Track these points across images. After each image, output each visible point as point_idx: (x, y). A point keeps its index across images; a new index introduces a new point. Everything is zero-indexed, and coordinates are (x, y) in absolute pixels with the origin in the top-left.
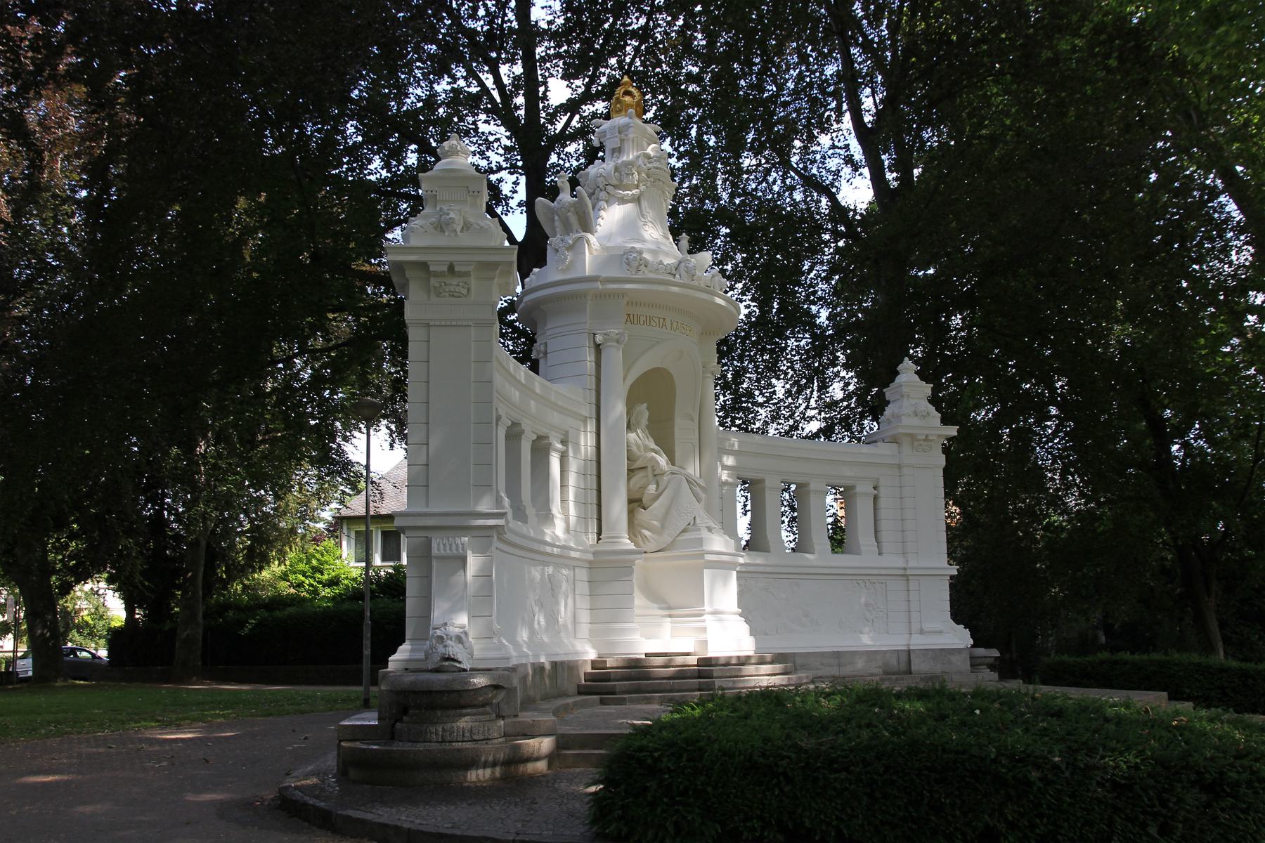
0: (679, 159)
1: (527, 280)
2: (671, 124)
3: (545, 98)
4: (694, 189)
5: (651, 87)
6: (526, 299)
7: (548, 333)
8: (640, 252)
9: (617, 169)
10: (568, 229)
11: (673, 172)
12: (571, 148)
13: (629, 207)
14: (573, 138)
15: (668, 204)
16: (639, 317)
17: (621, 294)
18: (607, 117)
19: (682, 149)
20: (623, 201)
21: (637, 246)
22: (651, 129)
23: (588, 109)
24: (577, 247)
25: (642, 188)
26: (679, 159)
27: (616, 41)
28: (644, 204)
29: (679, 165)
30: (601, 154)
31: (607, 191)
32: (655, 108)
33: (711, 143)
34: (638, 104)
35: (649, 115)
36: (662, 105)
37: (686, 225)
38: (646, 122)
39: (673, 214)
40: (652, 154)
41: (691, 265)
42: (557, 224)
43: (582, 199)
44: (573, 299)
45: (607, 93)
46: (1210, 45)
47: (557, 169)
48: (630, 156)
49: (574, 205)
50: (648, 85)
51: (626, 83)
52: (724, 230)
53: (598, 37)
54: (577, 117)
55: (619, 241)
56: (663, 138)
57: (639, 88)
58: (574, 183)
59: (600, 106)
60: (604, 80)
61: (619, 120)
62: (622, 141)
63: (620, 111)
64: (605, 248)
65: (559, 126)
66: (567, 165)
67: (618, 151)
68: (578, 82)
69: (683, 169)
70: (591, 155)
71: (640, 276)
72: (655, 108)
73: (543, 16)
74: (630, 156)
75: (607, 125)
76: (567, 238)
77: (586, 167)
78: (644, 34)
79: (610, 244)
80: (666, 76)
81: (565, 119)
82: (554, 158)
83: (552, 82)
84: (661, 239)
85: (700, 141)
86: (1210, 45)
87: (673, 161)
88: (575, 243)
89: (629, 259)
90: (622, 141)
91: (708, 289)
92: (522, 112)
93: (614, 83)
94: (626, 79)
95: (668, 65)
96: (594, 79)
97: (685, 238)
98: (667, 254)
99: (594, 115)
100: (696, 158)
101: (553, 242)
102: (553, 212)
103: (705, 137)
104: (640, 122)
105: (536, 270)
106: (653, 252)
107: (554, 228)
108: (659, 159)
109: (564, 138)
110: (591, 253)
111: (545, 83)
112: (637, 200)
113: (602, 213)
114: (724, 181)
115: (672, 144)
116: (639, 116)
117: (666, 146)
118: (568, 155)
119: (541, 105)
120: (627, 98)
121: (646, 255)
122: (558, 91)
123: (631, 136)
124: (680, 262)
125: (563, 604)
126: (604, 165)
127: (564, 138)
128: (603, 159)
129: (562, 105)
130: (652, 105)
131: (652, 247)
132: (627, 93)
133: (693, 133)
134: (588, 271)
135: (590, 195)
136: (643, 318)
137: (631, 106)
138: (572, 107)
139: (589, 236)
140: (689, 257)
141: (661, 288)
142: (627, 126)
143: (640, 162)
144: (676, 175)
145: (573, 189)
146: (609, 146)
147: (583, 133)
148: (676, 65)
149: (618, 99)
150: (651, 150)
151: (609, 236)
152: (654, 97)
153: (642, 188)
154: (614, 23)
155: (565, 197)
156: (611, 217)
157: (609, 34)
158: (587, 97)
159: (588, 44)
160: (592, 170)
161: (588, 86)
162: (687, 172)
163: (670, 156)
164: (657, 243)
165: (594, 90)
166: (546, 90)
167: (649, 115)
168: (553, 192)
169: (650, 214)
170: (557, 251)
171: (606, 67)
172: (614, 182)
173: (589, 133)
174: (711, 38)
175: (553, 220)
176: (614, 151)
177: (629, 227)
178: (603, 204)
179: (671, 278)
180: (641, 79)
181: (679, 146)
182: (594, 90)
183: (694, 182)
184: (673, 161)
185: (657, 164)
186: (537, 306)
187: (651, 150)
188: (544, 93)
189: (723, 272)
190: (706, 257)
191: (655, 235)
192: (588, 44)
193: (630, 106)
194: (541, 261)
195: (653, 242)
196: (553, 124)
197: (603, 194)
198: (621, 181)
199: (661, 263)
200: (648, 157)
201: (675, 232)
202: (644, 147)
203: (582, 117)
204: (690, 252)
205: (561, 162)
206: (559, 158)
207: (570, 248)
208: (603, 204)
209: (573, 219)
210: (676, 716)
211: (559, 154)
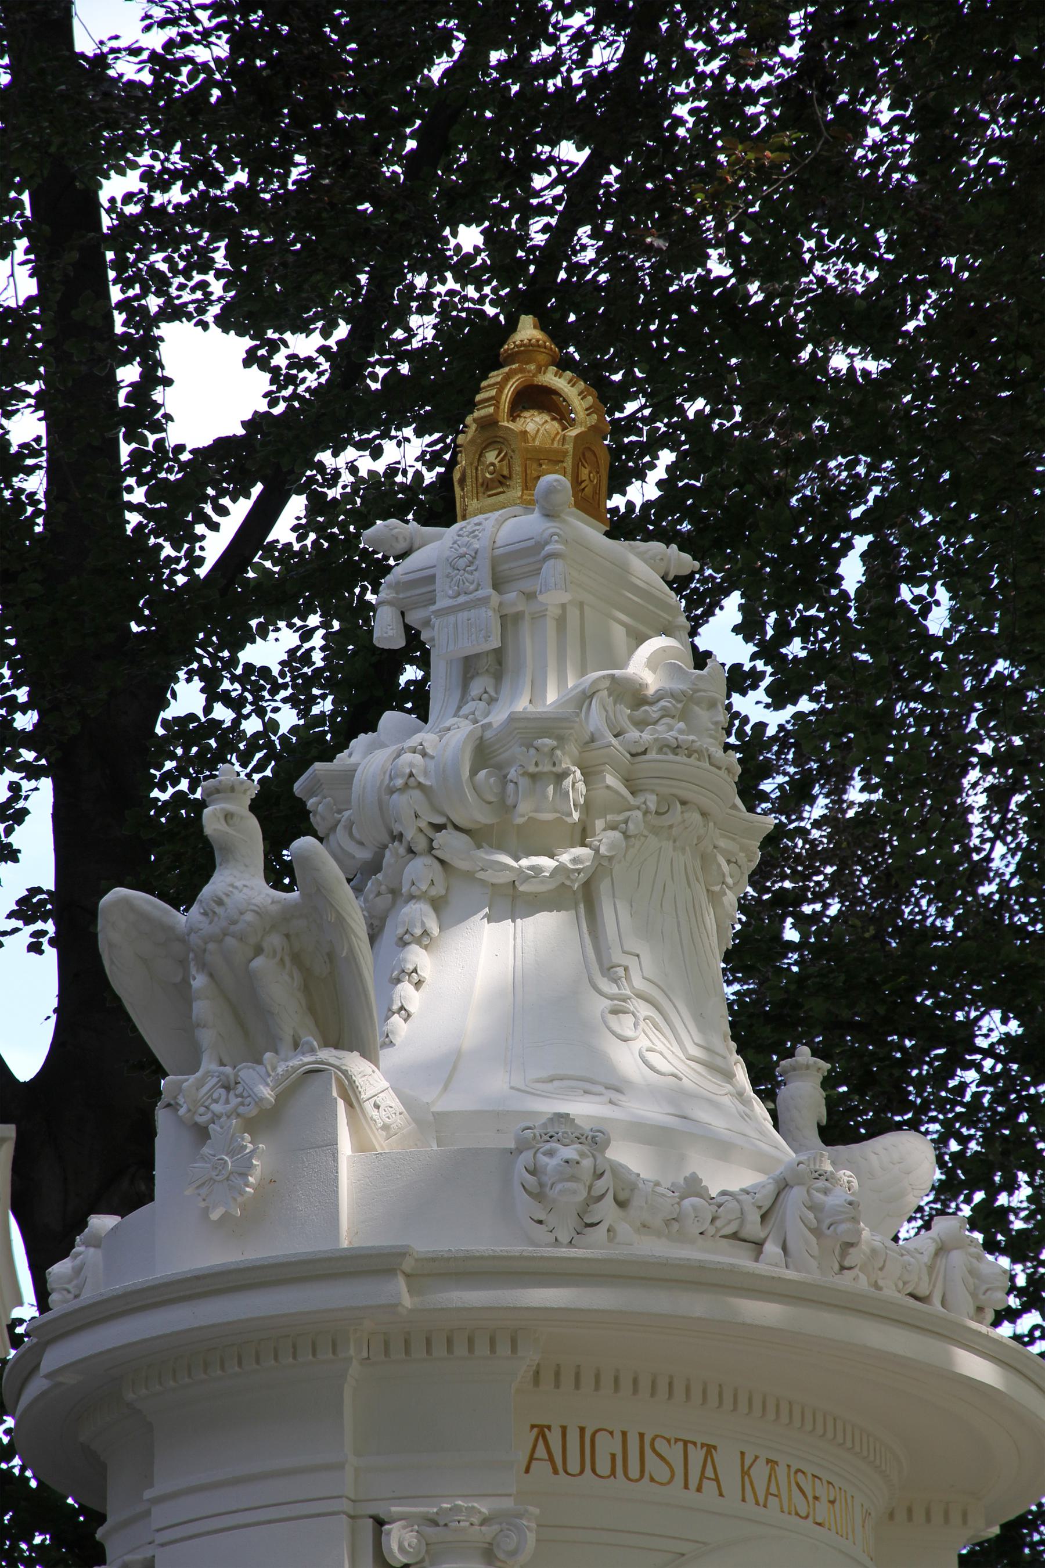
0: (779, 698)
1: (59, 1269)
2: (737, 531)
3: (145, 413)
4: (852, 834)
5: (653, 361)
6: (52, 1359)
7: (160, 1516)
8: (595, 1140)
9: (483, 753)
10: (253, 1032)
11: (753, 752)
12: (267, 652)
13: (544, 929)
14: (279, 602)
15: (721, 922)
16: (588, 1441)
17: (509, 1333)
18: (438, 506)
19: (795, 648)
20: (512, 901)
21: (584, 1109)
22: (647, 563)
23: (347, 463)
24: (298, 1114)
25: (606, 839)
26: (779, 698)
27: (482, 146)
28: (614, 915)
29: (776, 720)
30: (411, 673)
31: (443, 858)
32: (667, 457)
33: (937, 622)
34: (584, 448)
35: (643, 492)
36: (701, 447)
37: (817, 1006)
38: (623, 527)
39: (751, 952)
40: (652, 681)
41: (836, 1199)
42: (201, 1008)
43: (319, 896)
44: (284, 1354)
45: (442, 389)
46: (855, 954)
47: (206, 745)
48: (548, 691)
49: (281, 921)
50: (635, 349)
51: (529, 350)
52: (995, 1026)
53: (395, 128)
54: (296, 506)
55: (493, 1086)
56: (702, 605)
57: (592, 375)
58: (282, 815)
59: (406, 452)
60: (423, 327)
61: (494, 526)
62: (509, 622)
63: (502, 481)
64: (428, 1122)
65: (214, 546)
66: (252, 726)
67: (490, 667)
68: (304, 344)
69: (801, 736)
70: (368, 685)
71: (593, 1248)
72: (667, 457)
73: (131, 34)
74: (548, 691)
75: (435, 546)
76: (247, 1073)
77: (345, 736)
78: (619, 113)
79: (454, 1102)
80: (725, 303)
81: (240, 509)
82: (187, 698)
83: (177, 342)
84: (693, 1077)
85: (883, 614)
86: (855, 954)
87: (752, 705)
88: (285, 1097)
89: (542, 1170)
90: (509, 622)
91: (917, 1309)
92: (36, 483)
93: (474, 347)
94: (528, 330)
95: (731, 258)
96: (375, 319)
97: (806, 1077)
98: (723, 1149)
99: (382, 497)
100: (862, 693)
101: (186, 1092)
102: (183, 952)
103: (906, 593)
104: (593, 533)
105: (102, 1223)
106: (659, 1138)
107: (187, 1029)
108: (682, 705)
109: (235, 600)
110: (361, 1145)
111: (145, 349)
112: (581, 896)
113: (417, 957)
114: (998, 797)
115: (748, 629)
116: (589, 504)
117: (723, 637)
118: (257, 679)
119: (125, 450)
120: (535, 424)
121: (628, 1157)
122: (209, 384)
123: (553, 599)
124: (783, 1186)
125: (367, 1127)
126: (427, 737)
127: (235, 600)
128: (418, 701)
129: (223, 445)
130: (653, 446)
131: (654, 1113)
132: (535, 397)
133: (852, 572)
134: (350, 1228)
135: (359, 877)
136: (607, 1446)
137: (550, 459)
138: (267, 454)
139: (356, 1065)
140: (827, 1158)
141: (696, 1305)
142: (532, 554)
143: (596, 719)
144: (767, 771)
145: (276, 840)
146: (447, 643)
147: (330, 577)
148: (775, 263)
149: (489, 424)
150: (648, 662)
151: (448, 1067)
152: (664, 405)
153: (606, 839)
154: (474, 57)
155: (240, 883)
156: (462, 977)
157: (447, 110)
158: (340, 409)
159: (347, 161)
160: (368, 757)
161: (347, 362)
162: (821, 751)
163: (740, 680)
164: (677, 1096)
165: (377, 376)
166: (153, 377)
167: (643, 492)
168: (182, 863)
169: (642, 970)
170: (202, 1133)
171: (437, 268)
172: (474, 812)
173: (352, 575)
174: (937, 134)
175: (183, 992)
176: (469, 667)
177: (546, 1021)
178: (419, 914)
179: (741, 1259)
180: (602, 330)
181: (784, 634)
182: (377, 376)
183: (855, 794)
184: (752, 705)
185: (672, 731)
186: (106, 1387)
187: (648, 662)
188: (142, 390)
189: (989, 1219)
190: (910, 1158)
191: (664, 1053)
192: (347, 161)
193: (550, 459)
194: (128, 1184)
195: (653, 1093)
196: (184, 537)
197: (420, 871)
198: (505, 807)
199: (694, 1187)
200: (634, 696)
201: (760, 1036)
202: (603, 647)
203: (317, 504)
204: (837, 1131)
205: (222, 713)
206: (212, 694)
207: (265, 1121)
208: (419, 914)
209: (280, 989)
210: (169, 15)
211: (210, 680)
